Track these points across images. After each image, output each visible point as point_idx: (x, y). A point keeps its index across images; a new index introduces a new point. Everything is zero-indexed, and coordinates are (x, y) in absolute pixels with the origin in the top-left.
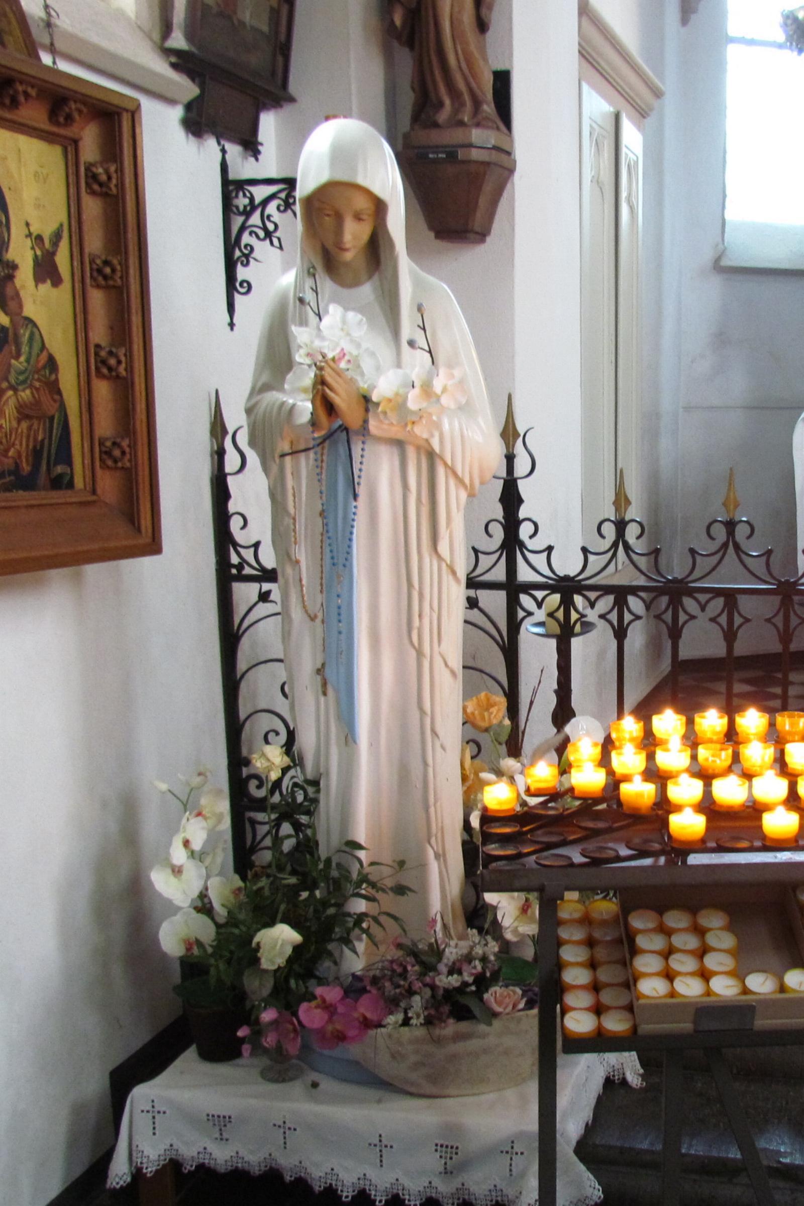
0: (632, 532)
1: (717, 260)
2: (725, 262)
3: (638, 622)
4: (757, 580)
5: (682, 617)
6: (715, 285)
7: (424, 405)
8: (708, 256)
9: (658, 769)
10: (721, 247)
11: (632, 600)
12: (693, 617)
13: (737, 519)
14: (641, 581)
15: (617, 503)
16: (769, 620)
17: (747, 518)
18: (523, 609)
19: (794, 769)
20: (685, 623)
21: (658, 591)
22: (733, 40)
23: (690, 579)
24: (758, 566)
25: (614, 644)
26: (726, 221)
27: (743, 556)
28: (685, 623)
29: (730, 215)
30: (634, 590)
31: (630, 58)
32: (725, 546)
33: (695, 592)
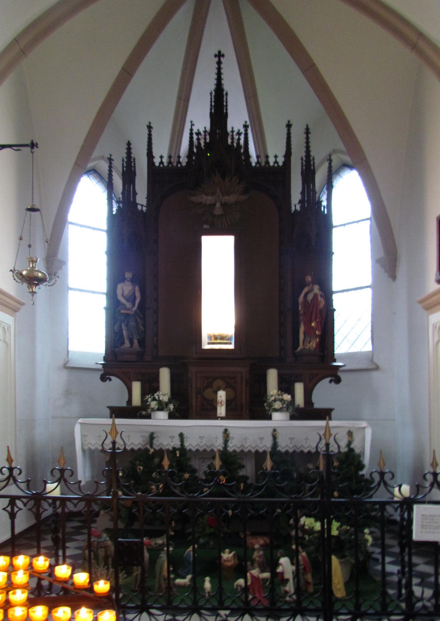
0: (16, 472)
1: (65, 364)
2: (68, 365)
3: (20, 512)
4: (73, 494)
5: (16, 509)
6: (64, 374)
7: (219, 403)
8: (62, 363)
9: (76, 587)
10: (67, 359)
11: (68, 503)
12: (20, 509)
13: (65, 468)
14: (20, 493)
15: (7, 460)
16: (4, 509)
17: (58, 467)
18: (17, 507)
19: (78, 583)
20: (17, 511)
21: (30, 498)
22: (71, 289)
23: (95, 494)
24: (23, 486)
25: (9, 521)
26: (69, 351)
27: (68, 484)
28: (17, 511)
29: (70, 348)
30: (19, 498)
31: (12, 297)
32: (8, 478)
33: (22, 498)
